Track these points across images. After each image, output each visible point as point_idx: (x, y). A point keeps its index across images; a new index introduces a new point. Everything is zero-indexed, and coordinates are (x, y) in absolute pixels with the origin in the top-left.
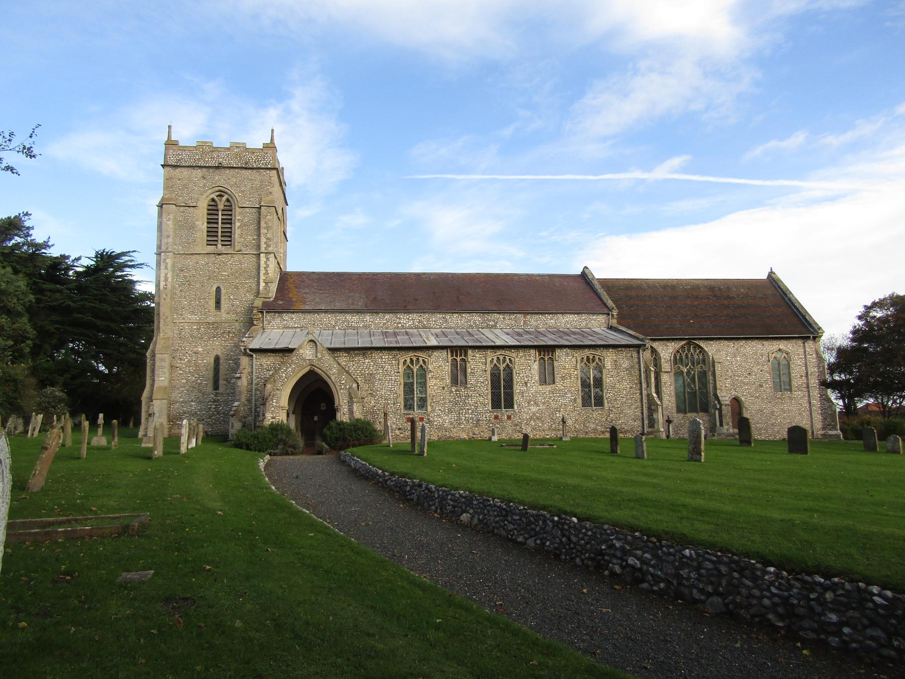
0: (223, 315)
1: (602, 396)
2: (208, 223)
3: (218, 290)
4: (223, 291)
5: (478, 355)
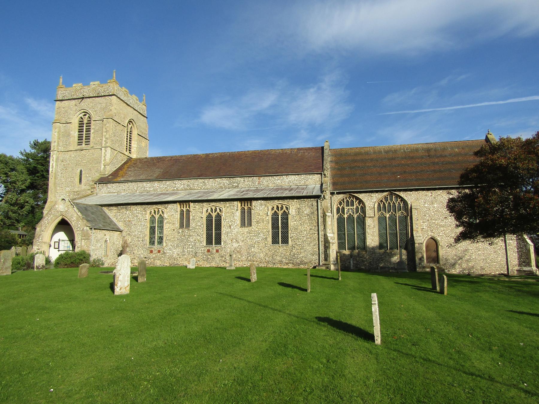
0: (83, 186)
1: (288, 236)
2: (79, 132)
3: (81, 171)
4: (83, 172)
5: (197, 205)
